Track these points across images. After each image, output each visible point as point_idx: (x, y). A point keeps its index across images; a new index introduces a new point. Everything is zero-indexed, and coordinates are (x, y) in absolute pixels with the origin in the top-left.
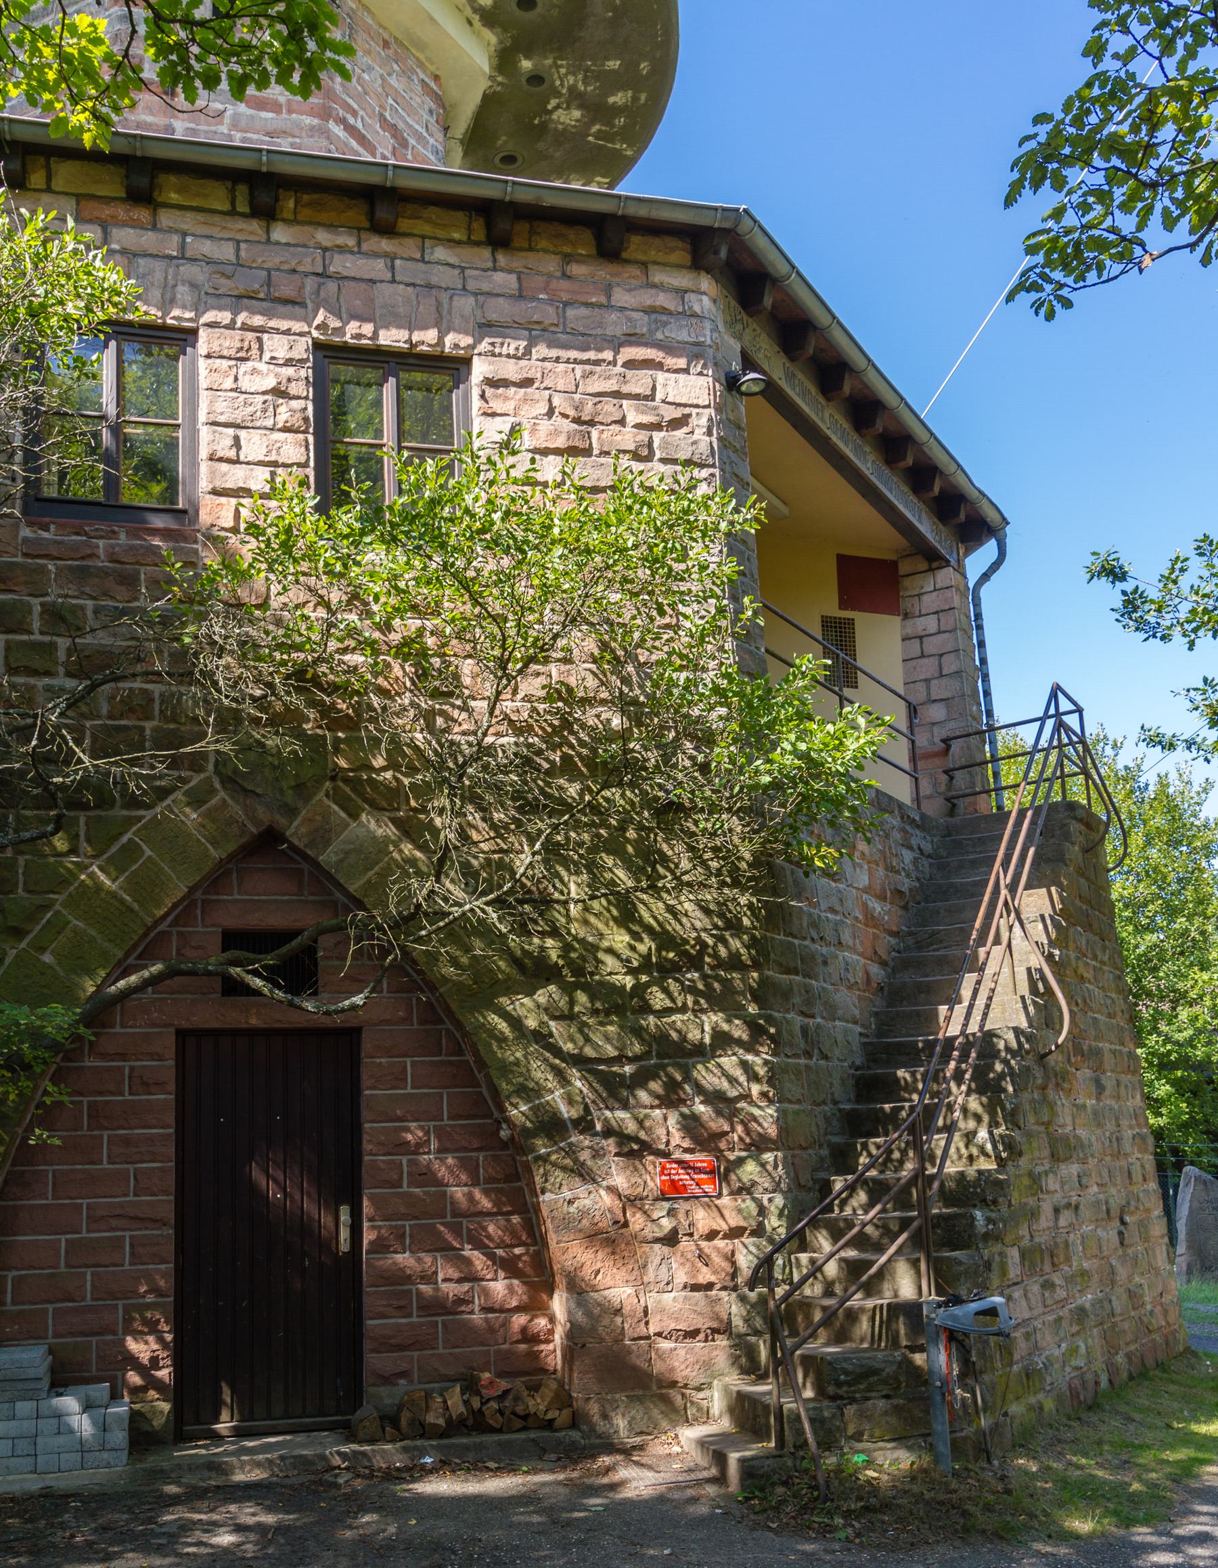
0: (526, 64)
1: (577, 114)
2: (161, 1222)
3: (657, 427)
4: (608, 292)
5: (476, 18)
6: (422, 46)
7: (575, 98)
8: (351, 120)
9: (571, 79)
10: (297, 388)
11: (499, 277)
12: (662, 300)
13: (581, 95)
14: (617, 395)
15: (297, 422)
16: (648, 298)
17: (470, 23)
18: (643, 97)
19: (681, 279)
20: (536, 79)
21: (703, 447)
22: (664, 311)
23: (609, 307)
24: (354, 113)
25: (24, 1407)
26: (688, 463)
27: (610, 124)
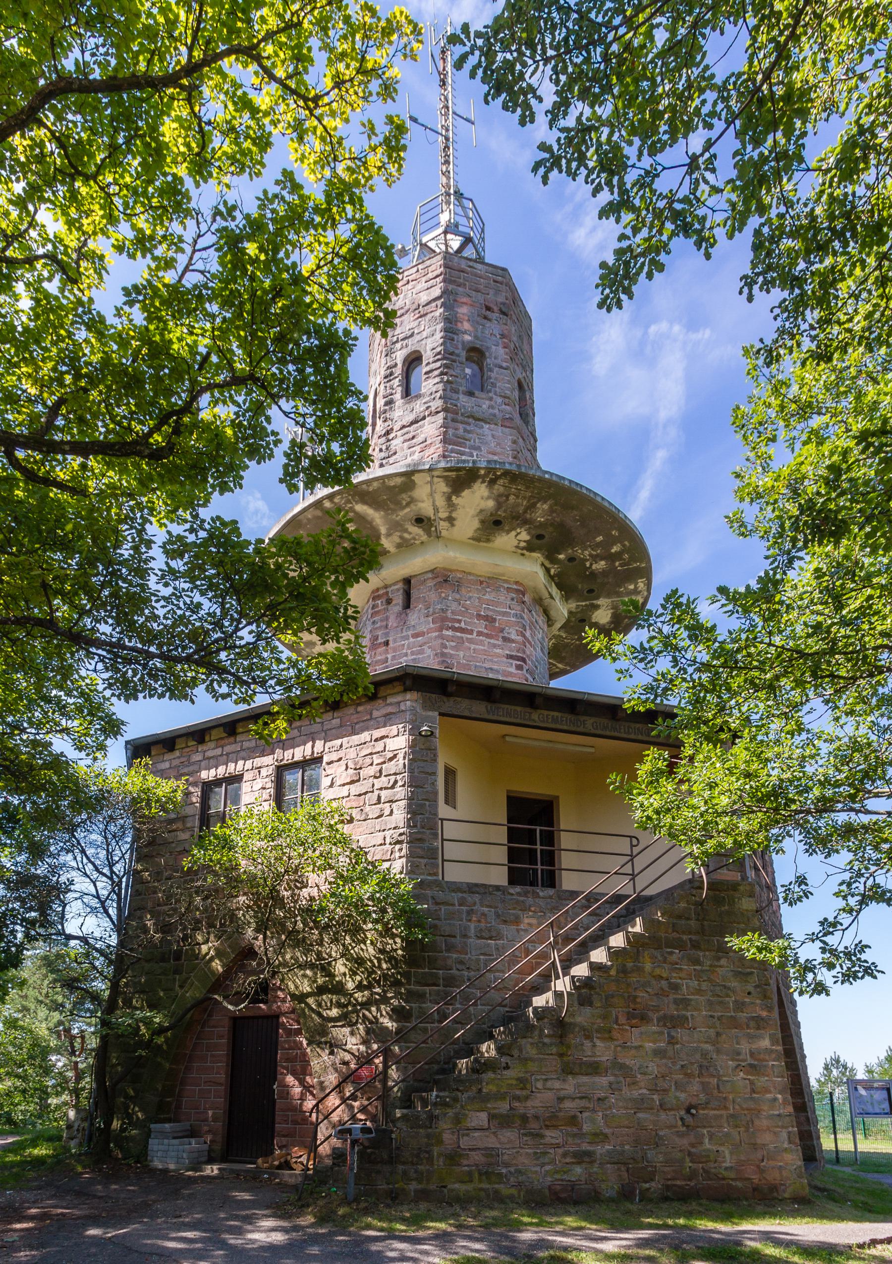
0: (562, 556)
1: (603, 563)
2: (221, 1084)
3: (384, 763)
4: (371, 714)
5: (525, 552)
6: (503, 575)
7: (595, 558)
8: (457, 625)
9: (587, 553)
10: (269, 785)
11: (334, 721)
12: (390, 709)
13: (597, 556)
14: (371, 754)
15: (268, 797)
16: (384, 711)
17: (523, 555)
18: (626, 543)
19: (399, 698)
20: (571, 559)
21: (401, 766)
22: (391, 713)
23: (371, 719)
24: (459, 621)
25: (166, 1141)
26: (395, 774)
27: (621, 559)
